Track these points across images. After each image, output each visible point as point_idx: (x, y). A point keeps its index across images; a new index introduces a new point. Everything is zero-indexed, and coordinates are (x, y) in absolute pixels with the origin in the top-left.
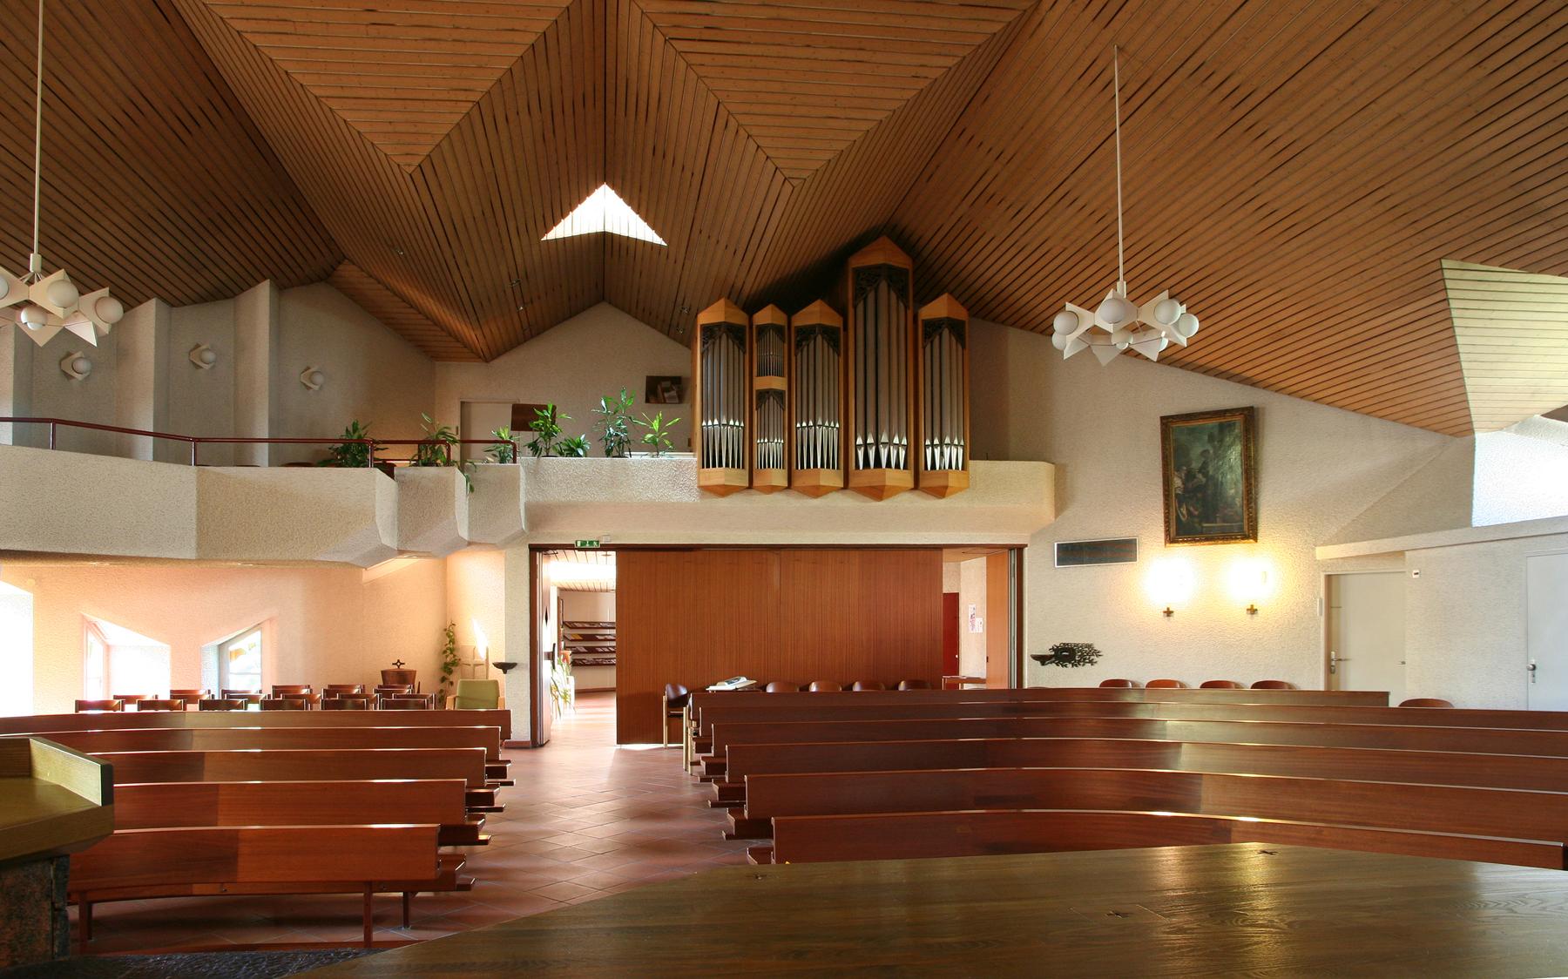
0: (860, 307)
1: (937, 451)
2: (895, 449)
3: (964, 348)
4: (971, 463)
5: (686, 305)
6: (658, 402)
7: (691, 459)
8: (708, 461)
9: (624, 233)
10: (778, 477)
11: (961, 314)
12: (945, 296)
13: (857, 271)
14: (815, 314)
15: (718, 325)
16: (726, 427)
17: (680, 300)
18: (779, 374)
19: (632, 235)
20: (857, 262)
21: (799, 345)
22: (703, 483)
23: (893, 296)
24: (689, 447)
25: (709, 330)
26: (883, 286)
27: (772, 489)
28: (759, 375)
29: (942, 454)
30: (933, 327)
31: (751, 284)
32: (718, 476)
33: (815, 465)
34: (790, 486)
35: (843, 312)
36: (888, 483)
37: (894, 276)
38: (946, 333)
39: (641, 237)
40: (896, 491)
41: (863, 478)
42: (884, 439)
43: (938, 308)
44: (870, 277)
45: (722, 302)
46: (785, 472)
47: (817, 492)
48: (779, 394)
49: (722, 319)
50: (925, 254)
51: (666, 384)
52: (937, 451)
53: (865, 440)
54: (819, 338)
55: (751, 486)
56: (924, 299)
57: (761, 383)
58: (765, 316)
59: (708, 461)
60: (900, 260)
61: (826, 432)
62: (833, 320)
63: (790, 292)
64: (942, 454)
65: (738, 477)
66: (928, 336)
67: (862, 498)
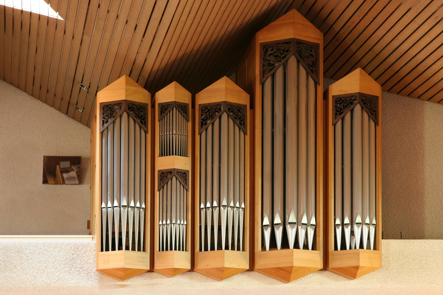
0: (339, 125)
1: (348, 231)
2: (303, 224)
3: (376, 124)
4: (384, 243)
5: (86, 83)
6: (56, 183)
7: (92, 241)
8: (109, 244)
9: (18, 7)
10: (181, 259)
11: (374, 89)
12: (357, 72)
13: (265, 47)
14: (221, 91)
15: (119, 103)
16: (127, 210)
17: (79, 77)
18: (183, 153)
19: (27, 9)
20: (265, 37)
21: (203, 123)
22: (103, 266)
23: (303, 72)
24: (88, 228)
25: (109, 110)
26: (292, 61)
27: (175, 272)
28: (161, 155)
29: (352, 233)
30: (344, 103)
31: (154, 58)
32: (118, 259)
33: (220, 247)
34: (193, 269)
35: (250, 89)
36: (296, 264)
37: (303, 52)
38: (358, 109)
39: (36, 11)
40: (304, 272)
41: (269, 259)
42: (292, 218)
43: (351, 84)
44: (278, 52)
45: (123, 79)
46: (146, 255)
47: (221, 274)
48: (183, 174)
49: (122, 97)
50: (337, 27)
51: (65, 164)
52: (348, 231)
53: (128, 203)
54: (225, 116)
55: (152, 269)
56: (336, 73)
57: (164, 163)
58: (169, 94)
59: (109, 244)
60: (311, 34)
61: (230, 212)
62: (240, 98)
63: (194, 70)
64: (352, 233)
65: (138, 260)
66: (339, 112)
67: (269, 279)
